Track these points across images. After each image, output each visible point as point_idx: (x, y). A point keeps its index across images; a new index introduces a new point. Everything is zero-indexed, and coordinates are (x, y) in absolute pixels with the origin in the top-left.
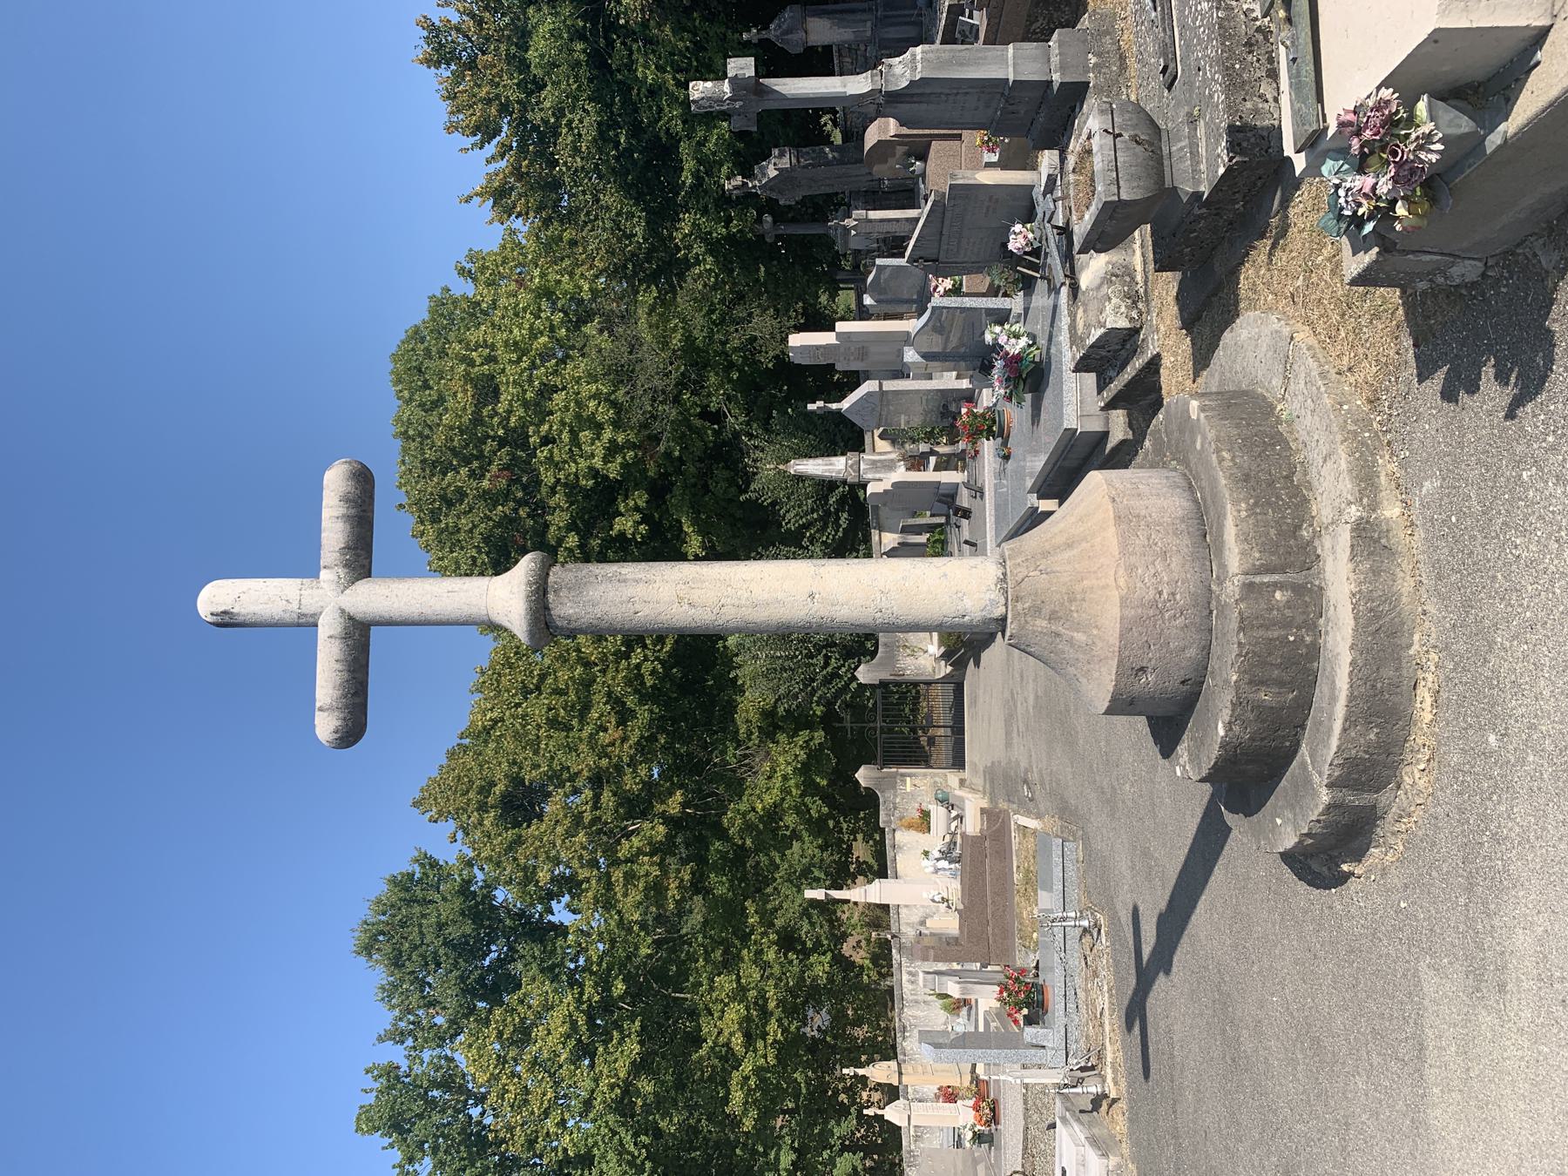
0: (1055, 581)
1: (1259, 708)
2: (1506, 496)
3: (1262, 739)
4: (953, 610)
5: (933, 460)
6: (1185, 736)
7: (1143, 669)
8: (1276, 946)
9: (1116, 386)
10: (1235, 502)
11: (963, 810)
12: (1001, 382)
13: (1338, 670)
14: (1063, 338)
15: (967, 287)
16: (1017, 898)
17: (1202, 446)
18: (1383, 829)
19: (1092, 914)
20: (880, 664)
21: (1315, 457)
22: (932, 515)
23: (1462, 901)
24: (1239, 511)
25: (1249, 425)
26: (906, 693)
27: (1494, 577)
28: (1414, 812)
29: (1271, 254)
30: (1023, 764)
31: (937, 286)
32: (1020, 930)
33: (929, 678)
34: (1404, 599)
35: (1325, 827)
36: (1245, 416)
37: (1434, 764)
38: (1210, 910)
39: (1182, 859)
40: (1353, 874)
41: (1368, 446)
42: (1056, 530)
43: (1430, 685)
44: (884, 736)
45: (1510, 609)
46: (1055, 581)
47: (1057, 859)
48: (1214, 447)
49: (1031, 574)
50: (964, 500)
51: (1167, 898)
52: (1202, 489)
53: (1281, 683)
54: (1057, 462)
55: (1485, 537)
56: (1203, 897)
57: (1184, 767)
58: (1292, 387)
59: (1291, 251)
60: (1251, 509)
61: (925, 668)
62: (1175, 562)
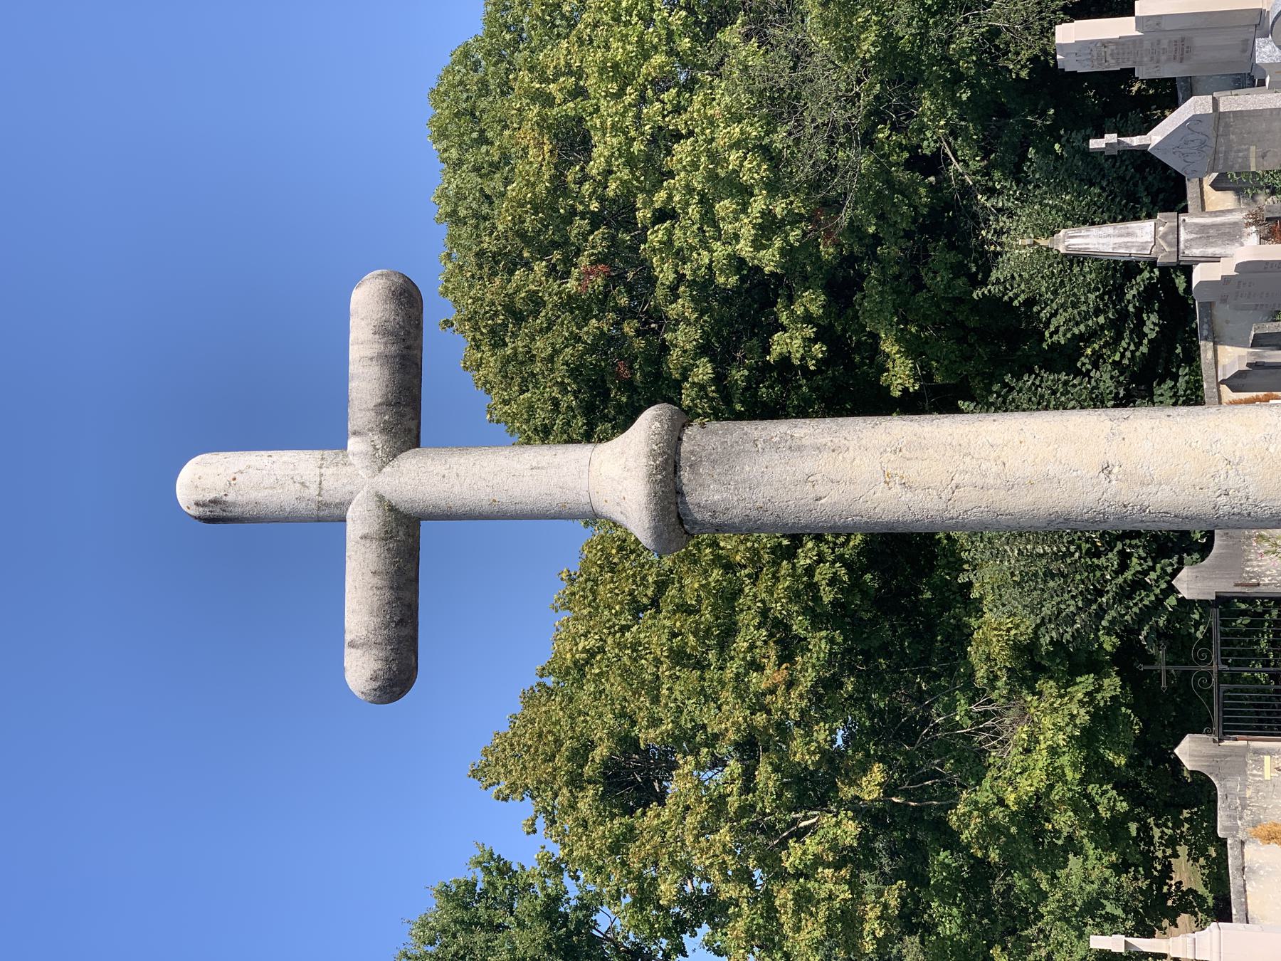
26: (1262, 615)
44: (1224, 686)
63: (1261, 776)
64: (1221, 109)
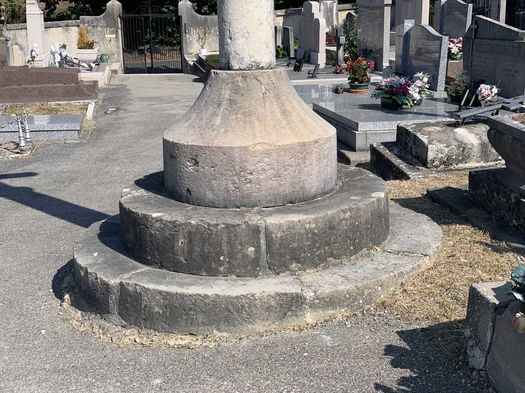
0: (259, 103)
1: (173, 238)
2: (323, 385)
3: (151, 242)
4: (236, 30)
5: (334, 49)
6: (151, 194)
7: (196, 163)
8: (13, 257)
9: (387, 153)
10: (315, 221)
11: (96, 71)
12: (390, 82)
13: (201, 287)
14: (422, 120)
15: (452, 63)
16: (38, 104)
17: (353, 200)
18: (95, 320)
19: (30, 149)
20: (192, 15)
21: (346, 271)
22: (295, 51)
23: (47, 366)
24: (309, 223)
25: (367, 229)
26: (173, 37)
27: (267, 379)
28: (107, 336)
29: (481, 243)
30: (129, 108)
31: (453, 43)
32: (17, 106)
33: (184, 51)
34: (250, 326)
35: (93, 283)
36: (373, 227)
37: (140, 347)
38: (36, 218)
39: (70, 201)
40: (63, 302)
41: (353, 302)
42: (295, 103)
43: (193, 343)
44: (143, 19)
45: (246, 389)
46: (259, 103)
47: (65, 126)
48: (354, 207)
49: (263, 87)
50: (306, 68)
51: (43, 193)
52: (324, 200)
53: (190, 252)
54: (335, 120)
55: (294, 373)
56: (44, 214)
57: (130, 193)
58: (392, 256)
59: (483, 255)
60: (311, 231)
61: (192, 48)
62: (273, 183)
63: (107, 34)
64: (385, 8)
